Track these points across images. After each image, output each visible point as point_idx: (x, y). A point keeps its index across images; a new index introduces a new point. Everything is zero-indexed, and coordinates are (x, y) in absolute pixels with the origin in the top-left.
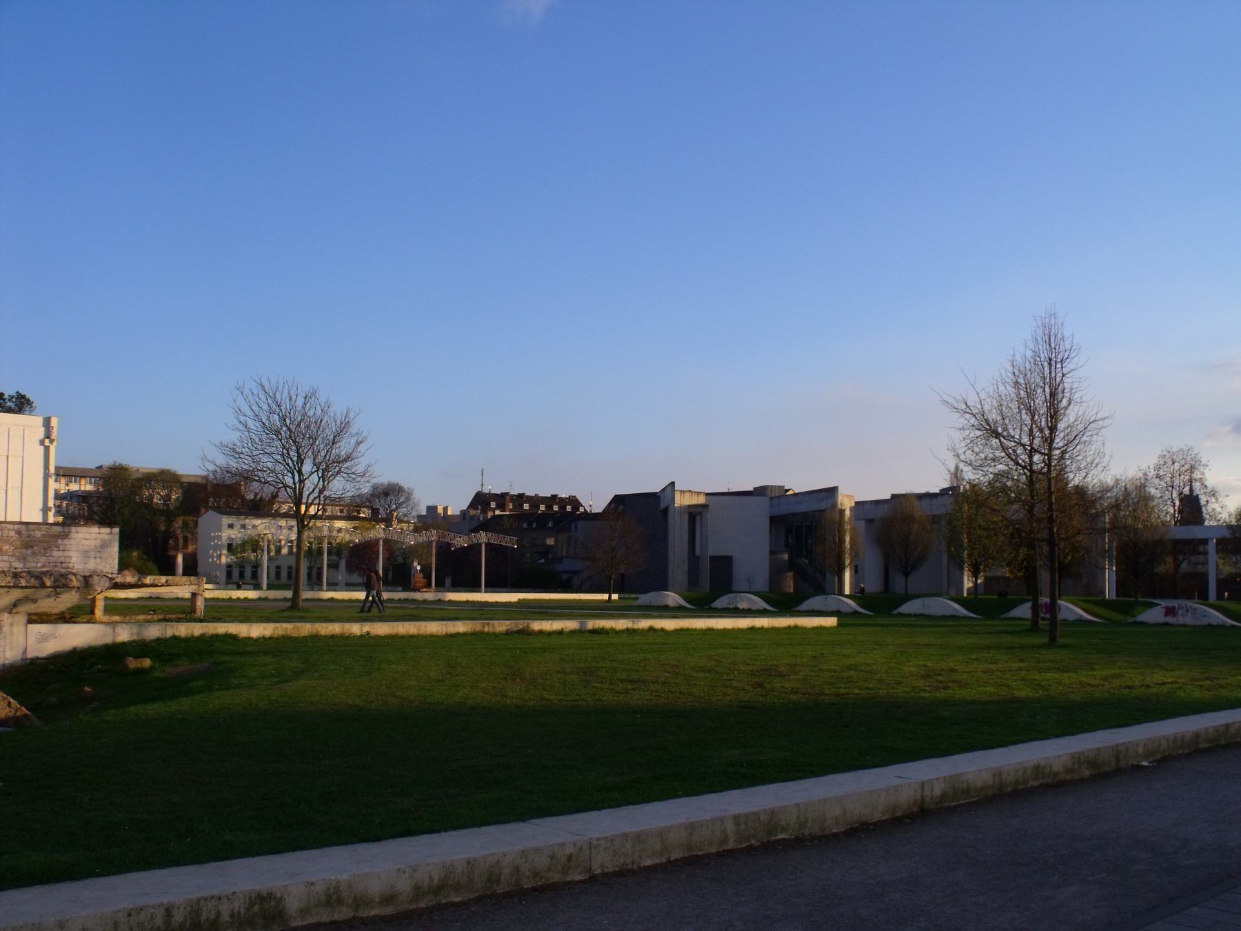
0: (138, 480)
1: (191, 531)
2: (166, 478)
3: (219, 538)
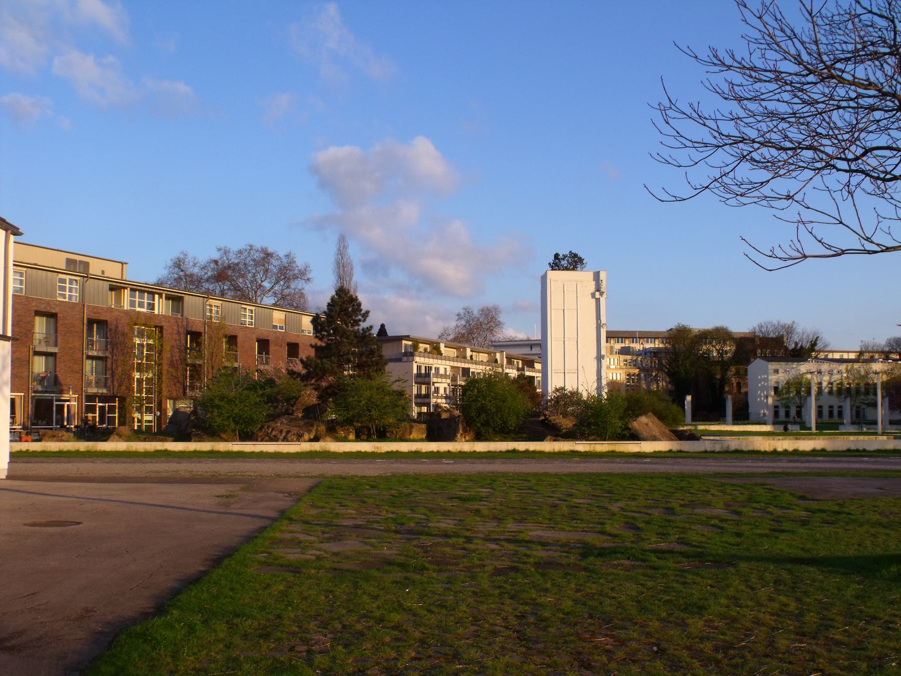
0: (696, 336)
1: (742, 375)
2: (720, 335)
3: (766, 380)
